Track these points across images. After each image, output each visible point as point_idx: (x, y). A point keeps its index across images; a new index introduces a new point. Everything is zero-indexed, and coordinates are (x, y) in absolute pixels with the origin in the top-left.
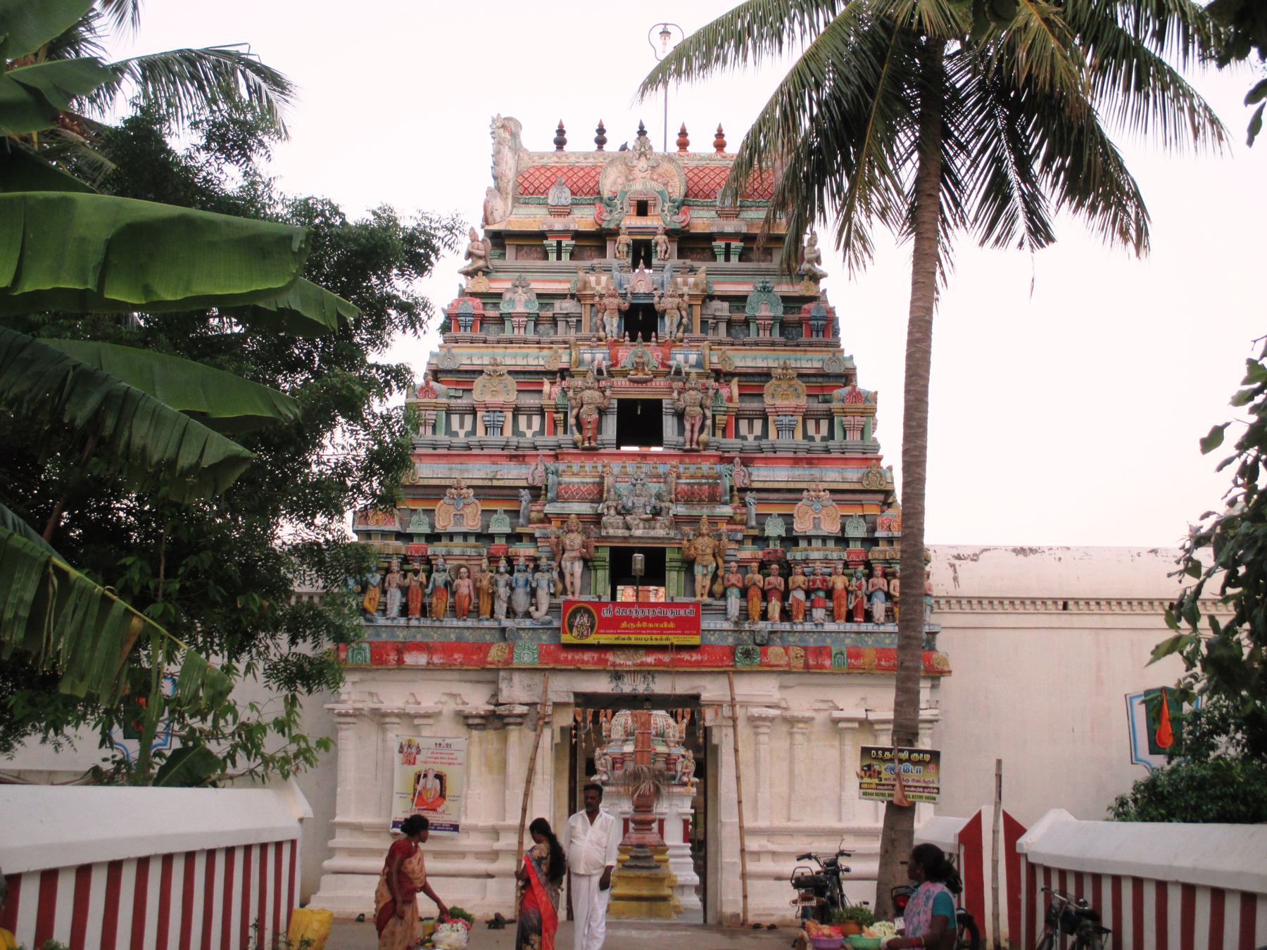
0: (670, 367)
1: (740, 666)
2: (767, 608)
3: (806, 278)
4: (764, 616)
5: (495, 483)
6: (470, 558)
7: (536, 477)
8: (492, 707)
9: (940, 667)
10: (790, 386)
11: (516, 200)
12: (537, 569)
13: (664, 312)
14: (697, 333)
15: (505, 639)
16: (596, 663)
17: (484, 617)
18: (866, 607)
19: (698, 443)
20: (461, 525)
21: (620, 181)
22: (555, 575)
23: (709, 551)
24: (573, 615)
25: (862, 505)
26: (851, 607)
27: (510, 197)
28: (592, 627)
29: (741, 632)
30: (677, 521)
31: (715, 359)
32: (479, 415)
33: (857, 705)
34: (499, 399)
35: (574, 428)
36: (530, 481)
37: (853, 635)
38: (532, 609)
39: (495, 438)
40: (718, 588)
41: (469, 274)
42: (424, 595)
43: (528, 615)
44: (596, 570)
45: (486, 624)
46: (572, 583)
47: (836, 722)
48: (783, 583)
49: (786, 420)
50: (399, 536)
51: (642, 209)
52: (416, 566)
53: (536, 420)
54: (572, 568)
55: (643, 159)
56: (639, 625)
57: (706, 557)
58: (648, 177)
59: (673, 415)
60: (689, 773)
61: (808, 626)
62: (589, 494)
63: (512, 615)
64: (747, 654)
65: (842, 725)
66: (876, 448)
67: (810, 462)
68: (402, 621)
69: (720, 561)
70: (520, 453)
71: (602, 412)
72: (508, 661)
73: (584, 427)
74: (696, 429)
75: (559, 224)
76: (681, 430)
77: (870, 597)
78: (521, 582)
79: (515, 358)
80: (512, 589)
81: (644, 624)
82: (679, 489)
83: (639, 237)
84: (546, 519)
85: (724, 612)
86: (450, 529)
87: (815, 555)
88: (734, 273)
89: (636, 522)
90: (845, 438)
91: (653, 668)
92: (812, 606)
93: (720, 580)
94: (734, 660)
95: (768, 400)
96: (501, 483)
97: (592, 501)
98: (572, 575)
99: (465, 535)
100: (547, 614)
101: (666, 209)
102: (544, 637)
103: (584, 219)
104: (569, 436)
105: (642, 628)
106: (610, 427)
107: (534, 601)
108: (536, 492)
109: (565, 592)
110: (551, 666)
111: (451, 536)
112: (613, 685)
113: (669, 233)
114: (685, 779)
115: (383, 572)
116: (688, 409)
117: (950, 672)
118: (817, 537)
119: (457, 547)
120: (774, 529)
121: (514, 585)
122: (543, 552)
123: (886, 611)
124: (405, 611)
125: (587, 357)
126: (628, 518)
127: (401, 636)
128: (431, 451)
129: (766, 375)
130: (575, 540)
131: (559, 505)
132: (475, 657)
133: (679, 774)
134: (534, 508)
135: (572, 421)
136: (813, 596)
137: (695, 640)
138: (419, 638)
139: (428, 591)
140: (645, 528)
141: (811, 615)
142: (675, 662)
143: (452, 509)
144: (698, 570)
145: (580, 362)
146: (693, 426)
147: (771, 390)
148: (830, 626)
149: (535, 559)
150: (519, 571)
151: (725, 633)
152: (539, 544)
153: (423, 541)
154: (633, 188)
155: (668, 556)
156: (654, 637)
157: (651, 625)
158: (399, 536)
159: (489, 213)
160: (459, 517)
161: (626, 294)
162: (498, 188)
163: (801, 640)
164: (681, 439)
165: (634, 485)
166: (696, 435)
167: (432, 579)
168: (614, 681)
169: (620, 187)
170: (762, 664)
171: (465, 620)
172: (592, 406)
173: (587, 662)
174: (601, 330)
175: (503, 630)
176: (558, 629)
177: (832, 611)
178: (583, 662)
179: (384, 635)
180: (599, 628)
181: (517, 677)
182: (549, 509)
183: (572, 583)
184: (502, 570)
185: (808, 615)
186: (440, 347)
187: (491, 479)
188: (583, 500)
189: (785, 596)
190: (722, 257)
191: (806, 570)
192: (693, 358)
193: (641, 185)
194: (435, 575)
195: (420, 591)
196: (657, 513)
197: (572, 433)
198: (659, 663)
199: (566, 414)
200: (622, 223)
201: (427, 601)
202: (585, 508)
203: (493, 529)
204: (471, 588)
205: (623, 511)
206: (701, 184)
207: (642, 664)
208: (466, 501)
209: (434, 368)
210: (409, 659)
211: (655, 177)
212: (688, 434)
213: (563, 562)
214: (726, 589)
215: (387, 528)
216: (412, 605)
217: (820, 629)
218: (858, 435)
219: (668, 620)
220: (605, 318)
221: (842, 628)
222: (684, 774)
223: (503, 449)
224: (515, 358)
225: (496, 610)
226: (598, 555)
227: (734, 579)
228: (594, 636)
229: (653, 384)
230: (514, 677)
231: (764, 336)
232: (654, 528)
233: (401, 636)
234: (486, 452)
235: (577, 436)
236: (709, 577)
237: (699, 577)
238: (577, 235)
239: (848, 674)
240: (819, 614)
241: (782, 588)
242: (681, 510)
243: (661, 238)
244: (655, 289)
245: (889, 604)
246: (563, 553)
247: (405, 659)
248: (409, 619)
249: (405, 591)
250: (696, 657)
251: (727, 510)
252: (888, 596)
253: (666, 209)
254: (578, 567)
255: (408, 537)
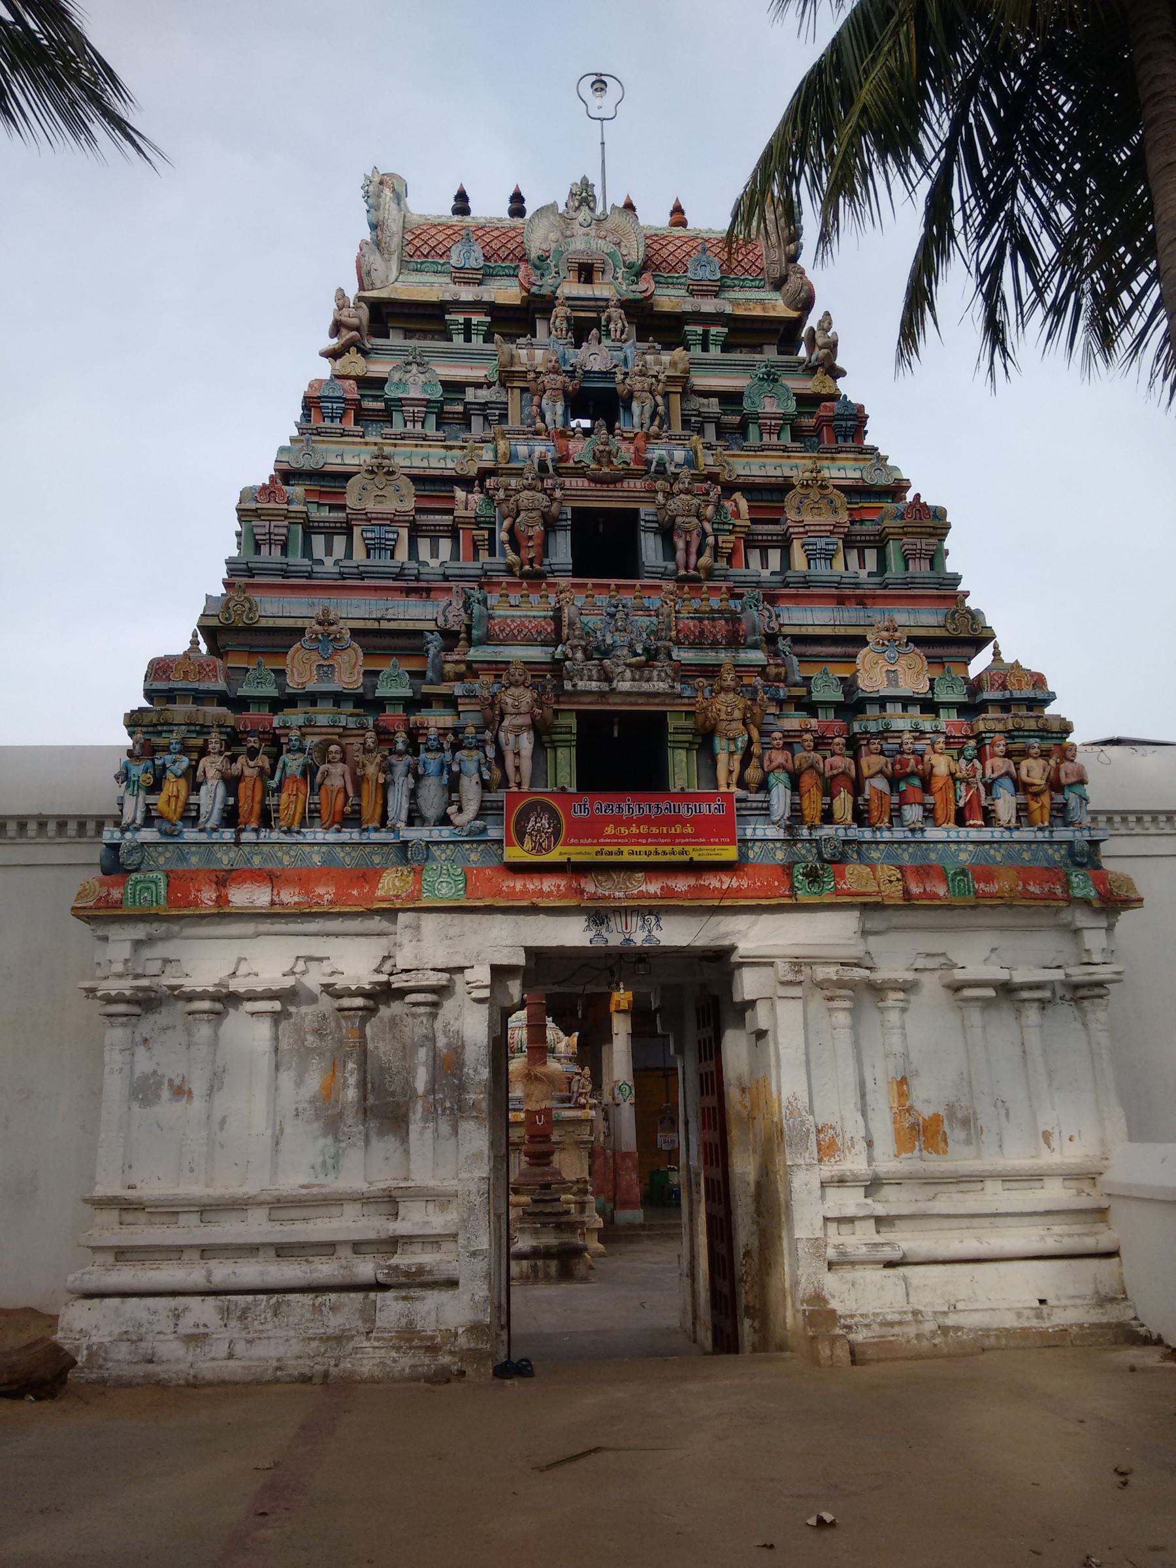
0: (648, 463)
1: (803, 897)
2: (831, 805)
3: (820, 369)
4: (828, 817)
5: (385, 625)
6: (345, 732)
7: (450, 616)
8: (383, 978)
9: (1123, 893)
10: (823, 496)
11: (403, 265)
12: (456, 747)
13: (631, 396)
14: (677, 429)
15: (405, 861)
16: (561, 897)
17: (371, 826)
18: (984, 803)
19: (696, 569)
20: (331, 680)
21: (553, 236)
22: (491, 752)
23: (737, 714)
24: (523, 818)
25: (943, 663)
26: (961, 804)
27: (395, 258)
28: (556, 833)
29: (796, 841)
30: (684, 673)
31: (707, 459)
32: (357, 531)
33: (986, 960)
34: (390, 506)
35: (507, 546)
36: (440, 622)
37: (971, 847)
38: (452, 810)
39: (381, 561)
40: (752, 773)
41: (333, 355)
42: (266, 792)
43: (445, 820)
44: (555, 749)
45: (375, 837)
46: (517, 768)
47: (957, 988)
48: (853, 767)
49: (821, 543)
50: (222, 699)
51: (586, 273)
52: (253, 742)
53: (445, 546)
54: (516, 742)
55: (585, 208)
56: (634, 830)
57: (734, 725)
58: (593, 233)
59: (656, 532)
60: (586, 1093)
61: (899, 834)
62: (539, 633)
63: (417, 821)
64: (813, 876)
65: (968, 993)
66: (956, 579)
67: (861, 601)
68: (228, 835)
69: (755, 734)
70: (423, 584)
71: (550, 524)
72: (415, 896)
73: (524, 544)
74: (693, 549)
75: (467, 294)
76: (669, 551)
77: (989, 787)
78: (433, 767)
79: (410, 457)
80: (418, 778)
81: (644, 829)
82: (681, 625)
83: (582, 314)
84: (472, 670)
85: (765, 811)
86: (311, 687)
87: (899, 724)
88: (715, 365)
89: (620, 669)
90: (907, 568)
91: (661, 902)
92: (903, 802)
93: (755, 761)
94: (792, 887)
95: (791, 515)
96: (393, 625)
97: (544, 644)
98: (517, 754)
99: (338, 698)
100: (476, 819)
101: (619, 275)
102: (473, 857)
103: (506, 292)
104: (498, 559)
105: (640, 836)
106: (562, 551)
107: (454, 797)
108: (450, 638)
109: (504, 782)
110: (488, 902)
111: (313, 698)
112: (590, 934)
113: (625, 305)
114: (583, 1101)
115: (195, 756)
116: (679, 520)
117: (1141, 900)
118: (894, 699)
119: (323, 715)
120: (827, 691)
121: (420, 771)
122: (470, 720)
123: (1018, 810)
124: (231, 818)
125: (522, 450)
126: (607, 662)
127: (225, 860)
128: (279, 580)
129: (783, 487)
130: (519, 698)
131: (490, 649)
132: (355, 892)
133: (575, 1095)
134: (449, 658)
135: (502, 536)
136: (903, 787)
137: (730, 853)
138: (257, 861)
139: (273, 784)
140: (634, 680)
141: (900, 817)
142: (698, 891)
143: (314, 656)
144: (720, 744)
145: (512, 457)
146: (688, 544)
147: (795, 502)
148: (932, 834)
149: (457, 731)
150: (428, 750)
151: (771, 845)
152: (461, 708)
153: (266, 710)
154: (571, 249)
155: (672, 723)
156: (660, 849)
157: (654, 830)
158: (222, 699)
159: (364, 270)
160: (326, 671)
161: (574, 371)
162: (378, 244)
163: (889, 856)
164: (671, 566)
165: (612, 616)
166: (693, 558)
167: (280, 765)
168: (592, 927)
169: (553, 245)
170: (838, 892)
171: (339, 831)
172: (535, 514)
173: (549, 894)
174: (538, 420)
175: (405, 843)
176: (499, 842)
177: (932, 811)
178: (541, 894)
179: (194, 860)
180: (568, 836)
181: (430, 922)
182: (475, 654)
183: (517, 768)
184: (400, 746)
185: (896, 816)
186: (292, 440)
187: (378, 620)
188: (530, 642)
189: (857, 788)
190: (699, 348)
191: (885, 746)
192: (679, 455)
193: (581, 244)
194: (285, 758)
195: (259, 785)
196: (652, 655)
197: (504, 554)
198: (668, 893)
199: (492, 532)
200: (558, 291)
201: (271, 801)
202: (537, 654)
203: (384, 690)
204: (348, 777)
205: (599, 652)
206: (665, 253)
207: (642, 896)
208: (336, 645)
209: (285, 466)
210: (241, 896)
211: (603, 233)
212: (680, 555)
213: (502, 734)
214: (766, 775)
215: (203, 686)
216: (244, 808)
217: (918, 836)
218: (925, 565)
219: (683, 822)
220: (544, 402)
221: (953, 836)
222: (581, 1094)
223: (394, 579)
224: (410, 457)
225: (391, 814)
226: (556, 722)
227: (779, 757)
228: (559, 848)
229: (625, 484)
230: (423, 923)
231: (770, 439)
232: (648, 680)
233: (225, 860)
234: (367, 582)
235: (512, 557)
236: (737, 757)
237: (722, 758)
238: (492, 309)
239: (973, 907)
240: (913, 813)
241: (853, 773)
242: (686, 656)
243: (616, 313)
244: (615, 366)
245: (1021, 799)
246: (502, 720)
247: (230, 898)
248: (239, 832)
249: (232, 783)
250: (726, 882)
251: (757, 656)
252: (1020, 786)
253: (619, 275)
254: (526, 743)
255: (240, 704)
